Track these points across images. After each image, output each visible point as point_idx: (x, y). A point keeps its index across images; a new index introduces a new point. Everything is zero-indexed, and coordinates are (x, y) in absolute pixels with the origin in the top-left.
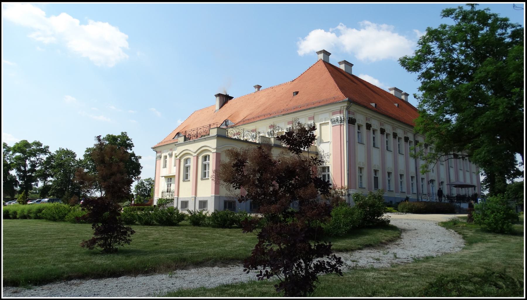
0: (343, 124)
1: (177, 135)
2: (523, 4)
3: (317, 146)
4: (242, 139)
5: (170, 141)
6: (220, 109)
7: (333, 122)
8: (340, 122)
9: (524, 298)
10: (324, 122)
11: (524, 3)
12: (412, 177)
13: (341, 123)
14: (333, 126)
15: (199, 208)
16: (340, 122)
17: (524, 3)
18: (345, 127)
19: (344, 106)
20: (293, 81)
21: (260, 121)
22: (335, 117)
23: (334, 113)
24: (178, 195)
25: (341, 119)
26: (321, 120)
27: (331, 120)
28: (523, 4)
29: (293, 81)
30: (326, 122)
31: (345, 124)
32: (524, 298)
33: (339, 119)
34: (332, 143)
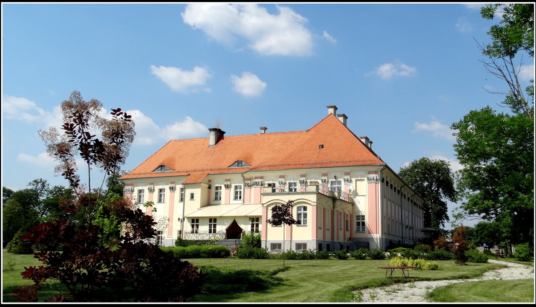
0: (378, 183)
1: (160, 168)
2: (3, 4)
3: (353, 198)
4: (490, 201)
5: (147, 173)
6: (216, 144)
7: (369, 179)
8: (375, 180)
9: (2, 303)
10: (360, 178)
11: (2, 3)
12: (389, 219)
13: (376, 181)
14: (368, 183)
15: (296, 249)
16: (375, 180)
17: (2, 3)
18: (379, 185)
19: (380, 169)
20: (308, 131)
21: (293, 170)
22: (371, 176)
23: (370, 173)
24: (266, 238)
25: (377, 178)
26: (357, 177)
27: (368, 178)
28: (3, 4)
29: (308, 131)
30: (362, 179)
31: (380, 183)
32: (2, 303)
33: (375, 178)
34: (367, 196)
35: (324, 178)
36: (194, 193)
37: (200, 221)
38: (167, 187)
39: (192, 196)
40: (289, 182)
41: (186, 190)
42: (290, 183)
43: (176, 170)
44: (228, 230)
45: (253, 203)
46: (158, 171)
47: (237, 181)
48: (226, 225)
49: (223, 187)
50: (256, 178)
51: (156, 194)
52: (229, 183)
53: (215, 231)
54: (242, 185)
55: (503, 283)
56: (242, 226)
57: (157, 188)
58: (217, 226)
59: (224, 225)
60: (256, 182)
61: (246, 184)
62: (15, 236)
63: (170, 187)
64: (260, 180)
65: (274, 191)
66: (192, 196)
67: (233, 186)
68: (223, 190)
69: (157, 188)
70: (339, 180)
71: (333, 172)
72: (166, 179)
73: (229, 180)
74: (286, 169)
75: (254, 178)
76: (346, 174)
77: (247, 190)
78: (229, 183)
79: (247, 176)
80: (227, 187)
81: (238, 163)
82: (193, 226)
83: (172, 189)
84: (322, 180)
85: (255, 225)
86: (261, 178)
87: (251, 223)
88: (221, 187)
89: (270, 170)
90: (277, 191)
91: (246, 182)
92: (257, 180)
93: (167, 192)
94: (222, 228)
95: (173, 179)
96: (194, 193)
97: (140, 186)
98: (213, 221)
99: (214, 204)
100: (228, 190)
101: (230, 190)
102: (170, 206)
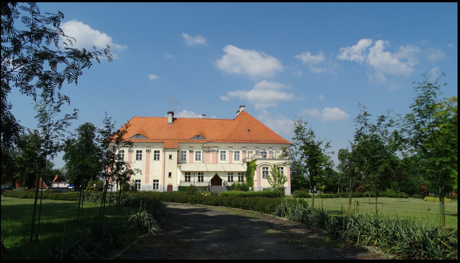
1: (136, 136)
10: (277, 151)
35: (244, 149)
36: (171, 155)
37: (234, 174)
38: (144, 150)
39: (170, 157)
40: (261, 151)
41: (166, 152)
42: (196, 151)
43: (150, 138)
44: (212, 180)
45: (211, 162)
46: (134, 137)
47: (198, 147)
48: (211, 177)
49: (188, 151)
50: (213, 147)
51: (134, 154)
52: (192, 149)
53: (202, 181)
54: (202, 151)
55: (38, 236)
56: (222, 178)
57: (135, 150)
58: (204, 177)
59: (209, 177)
60: (214, 150)
61: (204, 150)
62: (89, 183)
63: (147, 150)
64: (216, 149)
65: (265, 156)
66: (170, 157)
67: (195, 151)
68: (188, 153)
69: (153, 150)
70: (266, 151)
71: (262, 146)
72: (144, 144)
73: (192, 147)
74: (235, 143)
75: (211, 147)
76: (244, 147)
77: (206, 154)
78: (192, 149)
79: (205, 145)
80: (191, 152)
81: (198, 136)
82: (186, 177)
83: (148, 151)
84: (269, 151)
85: (241, 177)
86: (217, 147)
87: (228, 176)
88: (186, 151)
89: (224, 143)
90: (268, 157)
91: (204, 149)
92: (214, 149)
93: (144, 154)
94: (207, 179)
95: (149, 144)
96: (171, 155)
97: (156, 148)
98: (201, 175)
99: (181, 162)
100: (191, 154)
101: (193, 154)
102: (147, 163)
